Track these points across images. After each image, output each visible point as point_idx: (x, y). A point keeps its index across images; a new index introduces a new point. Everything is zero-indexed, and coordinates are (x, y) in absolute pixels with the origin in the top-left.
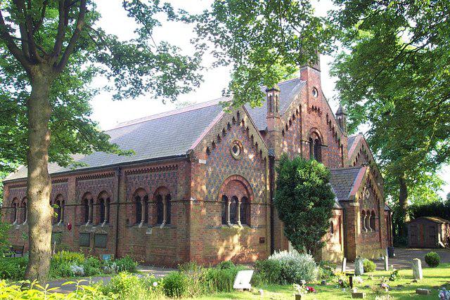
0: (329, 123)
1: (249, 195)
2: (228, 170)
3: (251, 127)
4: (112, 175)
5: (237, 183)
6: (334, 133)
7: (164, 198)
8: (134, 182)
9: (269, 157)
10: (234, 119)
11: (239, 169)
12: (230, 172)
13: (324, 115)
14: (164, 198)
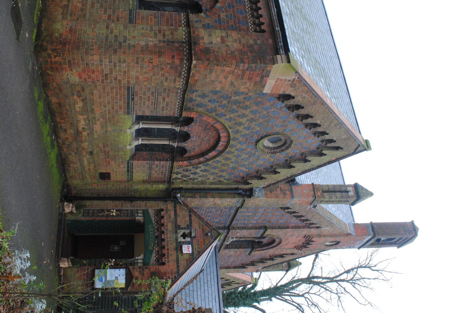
1: (189, 158)
3: (308, 165)
5: (212, 142)
10: (331, 141)
12: (237, 132)
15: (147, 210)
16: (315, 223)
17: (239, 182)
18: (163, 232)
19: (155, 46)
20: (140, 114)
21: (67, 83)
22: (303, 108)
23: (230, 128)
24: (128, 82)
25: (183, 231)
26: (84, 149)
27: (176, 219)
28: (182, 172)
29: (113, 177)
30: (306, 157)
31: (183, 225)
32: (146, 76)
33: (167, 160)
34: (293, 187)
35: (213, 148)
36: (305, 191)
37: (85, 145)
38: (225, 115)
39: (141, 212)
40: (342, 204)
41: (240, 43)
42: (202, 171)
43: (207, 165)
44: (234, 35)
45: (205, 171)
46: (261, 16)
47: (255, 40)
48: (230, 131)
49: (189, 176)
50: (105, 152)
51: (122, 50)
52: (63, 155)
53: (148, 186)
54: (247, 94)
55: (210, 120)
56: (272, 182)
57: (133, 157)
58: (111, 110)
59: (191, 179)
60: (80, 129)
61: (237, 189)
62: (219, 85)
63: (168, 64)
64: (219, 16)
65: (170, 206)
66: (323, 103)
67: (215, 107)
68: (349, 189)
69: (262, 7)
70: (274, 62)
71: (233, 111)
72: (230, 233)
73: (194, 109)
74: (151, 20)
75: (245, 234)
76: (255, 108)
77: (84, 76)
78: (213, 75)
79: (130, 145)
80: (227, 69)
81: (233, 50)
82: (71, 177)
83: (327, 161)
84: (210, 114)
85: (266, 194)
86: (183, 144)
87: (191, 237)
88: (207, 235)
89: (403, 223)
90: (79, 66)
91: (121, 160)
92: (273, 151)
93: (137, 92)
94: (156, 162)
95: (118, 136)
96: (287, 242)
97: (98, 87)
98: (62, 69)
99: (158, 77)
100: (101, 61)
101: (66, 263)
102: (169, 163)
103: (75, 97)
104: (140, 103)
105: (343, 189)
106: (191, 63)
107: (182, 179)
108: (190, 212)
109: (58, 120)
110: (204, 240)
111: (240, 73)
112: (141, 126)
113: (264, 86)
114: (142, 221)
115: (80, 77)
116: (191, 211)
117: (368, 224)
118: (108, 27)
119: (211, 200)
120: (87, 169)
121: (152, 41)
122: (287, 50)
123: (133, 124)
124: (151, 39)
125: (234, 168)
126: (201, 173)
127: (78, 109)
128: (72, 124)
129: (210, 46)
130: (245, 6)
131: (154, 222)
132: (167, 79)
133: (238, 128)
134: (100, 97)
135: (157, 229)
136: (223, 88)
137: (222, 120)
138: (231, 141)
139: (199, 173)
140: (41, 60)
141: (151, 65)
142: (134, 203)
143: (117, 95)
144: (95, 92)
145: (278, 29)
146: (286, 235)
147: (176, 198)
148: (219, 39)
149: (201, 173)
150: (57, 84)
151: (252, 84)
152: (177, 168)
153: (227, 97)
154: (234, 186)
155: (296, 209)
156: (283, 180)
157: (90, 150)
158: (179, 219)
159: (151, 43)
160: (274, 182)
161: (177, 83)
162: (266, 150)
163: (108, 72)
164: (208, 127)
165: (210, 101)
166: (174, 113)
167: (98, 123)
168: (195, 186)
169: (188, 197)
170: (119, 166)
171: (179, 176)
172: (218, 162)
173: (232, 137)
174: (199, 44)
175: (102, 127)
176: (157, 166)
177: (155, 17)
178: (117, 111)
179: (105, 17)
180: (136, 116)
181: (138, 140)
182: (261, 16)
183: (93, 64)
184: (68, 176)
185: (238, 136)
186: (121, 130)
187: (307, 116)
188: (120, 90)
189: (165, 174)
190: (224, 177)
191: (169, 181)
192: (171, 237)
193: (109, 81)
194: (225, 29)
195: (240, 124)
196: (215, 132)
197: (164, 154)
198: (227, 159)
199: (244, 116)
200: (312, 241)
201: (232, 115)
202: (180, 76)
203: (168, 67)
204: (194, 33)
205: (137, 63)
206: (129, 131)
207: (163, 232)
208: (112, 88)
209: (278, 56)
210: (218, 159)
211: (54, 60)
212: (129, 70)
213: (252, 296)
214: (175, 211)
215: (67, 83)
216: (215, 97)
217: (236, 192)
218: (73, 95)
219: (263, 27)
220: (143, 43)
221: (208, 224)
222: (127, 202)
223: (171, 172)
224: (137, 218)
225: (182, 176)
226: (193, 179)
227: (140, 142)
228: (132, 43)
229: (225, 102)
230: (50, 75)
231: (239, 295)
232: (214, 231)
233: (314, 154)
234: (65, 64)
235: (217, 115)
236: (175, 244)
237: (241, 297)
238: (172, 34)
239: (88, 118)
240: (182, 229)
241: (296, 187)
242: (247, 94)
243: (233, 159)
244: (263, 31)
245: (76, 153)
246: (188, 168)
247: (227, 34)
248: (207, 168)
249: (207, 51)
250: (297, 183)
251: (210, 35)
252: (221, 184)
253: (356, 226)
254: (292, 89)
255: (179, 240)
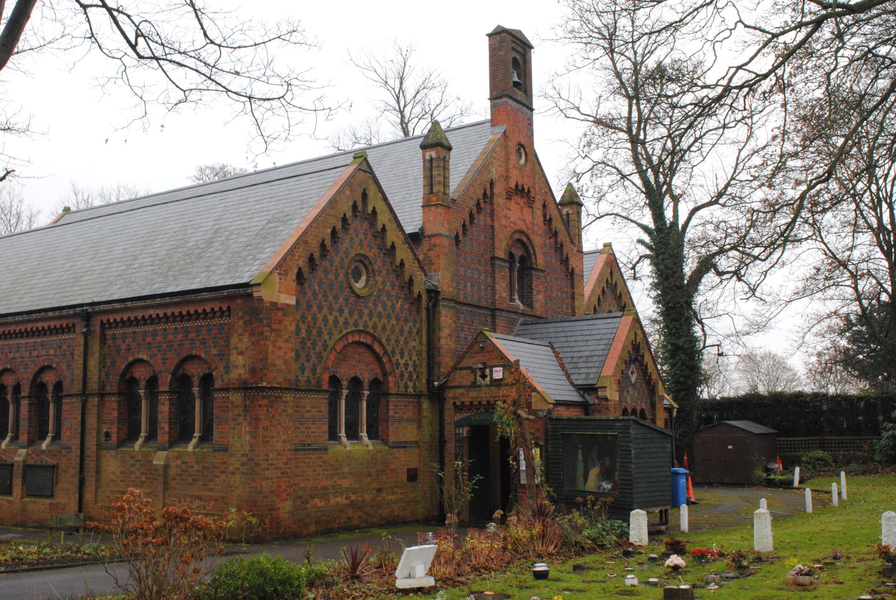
0: (548, 221)
1: (385, 374)
2: (341, 320)
3: (391, 227)
4: (70, 329)
5: (361, 350)
6: (556, 242)
7: (196, 381)
8: (123, 347)
9: (429, 291)
10: (355, 207)
11: (366, 318)
12: (346, 323)
13: (538, 205)
14: (196, 381)
15: (455, 422)
16: (483, 191)
17: (418, 308)
18: (480, 402)
19: (249, 424)
20: (327, 436)
21: (293, 513)
22: (312, 255)
23: (341, 332)
24: (289, 450)
25: (478, 378)
26: (374, 499)
27: (464, 387)
28: (404, 382)
29: (413, 465)
30: (378, 232)
31: (472, 378)
32: (281, 433)
33: (388, 402)
34: (426, 234)
35: (369, 347)
36: (431, 218)
37: (368, 497)
38: (325, 341)
39: (457, 430)
40: (449, 166)
41: (242, 335)
42: (402, 357)
43: (393, 352)
44: (234, 340)
45: (402, 353)
46: (212, 309)
47: (239, 318)
48: (345, 332)
49: (411, 372)
50: (377, 475)
51: (255, 457)
52: (382, 522)
53: (425, 422)
54: (298, 321)
55: (332, 357)
56: (417, 265)
57: (385, 442)
58: (323, 468)
59: (415, 370)
60: (347, 502)
61: (427, 309)
62: (289, 355)
63: (267, 411)
64: (215, 355)
65: (450, 394)
66: (306, 232)
67: (316, 353)
68: (428, 157)
69: (202, 308)
70: (260, 300)
71: (320, 333)
72: (501, 307)
73: (319, 378)
74: (224, 428)
75: (504, 286)
76: (315, 308)
77: (284, 496)
78: (277, 362)
79: (367, 446)
80: (270, 349)
81: (250, 344)
82: (413, 514)
83: (384, 203)
84: (324, 358)
85: (435, 270)
86: (365, 384)
87: (485, 368)
88: (482, 348)
89: (490, 50)
90: (274, 501)
91: (389, 456)
92: (371, 274)
93: (300, 441)
94: (391, 413)
95: (356, 460)
96: (519, 222)
97: (296, 482)
98: (277, 518)
99: (282, 420)
100: (268, 478)
101: (512, 518)
102: (391, 399)
103: (309, 506)
104: (314, 437)
105: (428, 165)
106: (266, 388)
107: (416, 380)
108: (456, 369)
109: (337, 526)
110: (488, 352)
111: (274, 334)
112: (343, 434)
113: (288, 305)
114: (468, 428)
115: (286, 499)
116: (455, 368)
117: (491, 105)
118: (233, 473)
119: (443, 341)
120: (402, 496)
121: (245, 428)
122: (246, 285)
123: (341, 443)
124: (243, 429)
125: (397, 318)
126: (406, 357)
127: (323, 504)
128: (341, 511)
129: (247, 367)
130: (202, 326)
131: (469, 414)
132: (284, 411)
133: (341, 323)
134: (308, 480)
135: (477, 409)
136: (292, 350)
137: (331, 344)
138: (358, 328)
139: (406, 361)
140: (269, 538)
141: (270, 428)
142: (447, 439)
143: (305, 463)
144: (302, 485)
145: (225, 293)
146: (506, 227)
147: (440, 386)
148: (240, 357)
149: (406, 357)
150: (295, 524)
151: (286, 318)
152: (399, 387)
153: (303, 343)
154: (424, 313)
155: (458, 225)
156: (413, 251)
157: (375, 492)
158: (464, 383)
159: (248, 429)
160: (416, 262)
161: (288, 399)
162: (371, 283)
163: (280, 472)
164: (342, 356)
165: (308, 361)
166: (324, 399)
167: (339, 482)
168: (425, 364)
169: (439, 370)
170: (397, 458)
171: (410, 384)
172: (388, 340)
173: (354, 329)
174: (246, 379)
175: (344, 478)
176: (395, 413)
177: (220, 424)
178: (324, 462)
179: (223, 477)
180: (330, 440)
181: (362, 437)
182: (212, 309)
183: (271, 487)
184: (411, 519)
185: (351, 322)
186: (348, 457)
187: (323, 246)
188: (299, 459)
189: (408, 402)
190: (411, 328)
191: (418, 396)
192: (485, 394)
193: (289, 470)
194: (229, 350)
195: (336, 321)
196: (348, 348)
197: (381, 405)
198: (384, 328)
199: (325, 320)
200: (517, 186)
201: (325, 333)
202: (280, 397)
203: (270, 410)
204: (234, 384)
205: (268, 442)
206: (348, 449)
207: (480, 402)
208: (297, 467)
209: (255, 295)
210: (384, 340)
211: (268, 526)
212: (276, 450)
213: (663, 235)
214: (456, 387)
215: (293, 513)
216: (303, 355)
217: (431, 311)
218: (306, 508)
219: (225, 309)
220: (248, 437)
221: (470, 347)
222: (446, 447)
223: (404, 395)
224: (465, 435)
225: (411, 381)
226: (415, 366)
227: (364, 434)
228: (247, 448)
229: (309, 344)
230: (285, 531)
231: (660, 257)
232: (478, 338)
233: (374, 221)
234: (272, 515)
235: (325, 350)
236: (493, 388)
237: (663, 253)
238: (237, 407)
239: (333, 493)
240: (476, 379)
241: (426, 230)
242: (298, 321)
243: (384, 321)
244: (229, 308)
245: (380, 508)
246: (398, 375)
247: (233, 348)
248: (398, 352)
249: (253, 371)
250: (422, 229)
251: (236, 367)
252: (422, 330)
253: (494, 122)
254: (290, 273)
255: (489, 383)
